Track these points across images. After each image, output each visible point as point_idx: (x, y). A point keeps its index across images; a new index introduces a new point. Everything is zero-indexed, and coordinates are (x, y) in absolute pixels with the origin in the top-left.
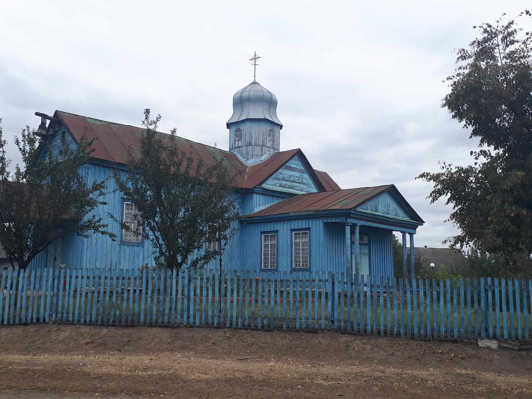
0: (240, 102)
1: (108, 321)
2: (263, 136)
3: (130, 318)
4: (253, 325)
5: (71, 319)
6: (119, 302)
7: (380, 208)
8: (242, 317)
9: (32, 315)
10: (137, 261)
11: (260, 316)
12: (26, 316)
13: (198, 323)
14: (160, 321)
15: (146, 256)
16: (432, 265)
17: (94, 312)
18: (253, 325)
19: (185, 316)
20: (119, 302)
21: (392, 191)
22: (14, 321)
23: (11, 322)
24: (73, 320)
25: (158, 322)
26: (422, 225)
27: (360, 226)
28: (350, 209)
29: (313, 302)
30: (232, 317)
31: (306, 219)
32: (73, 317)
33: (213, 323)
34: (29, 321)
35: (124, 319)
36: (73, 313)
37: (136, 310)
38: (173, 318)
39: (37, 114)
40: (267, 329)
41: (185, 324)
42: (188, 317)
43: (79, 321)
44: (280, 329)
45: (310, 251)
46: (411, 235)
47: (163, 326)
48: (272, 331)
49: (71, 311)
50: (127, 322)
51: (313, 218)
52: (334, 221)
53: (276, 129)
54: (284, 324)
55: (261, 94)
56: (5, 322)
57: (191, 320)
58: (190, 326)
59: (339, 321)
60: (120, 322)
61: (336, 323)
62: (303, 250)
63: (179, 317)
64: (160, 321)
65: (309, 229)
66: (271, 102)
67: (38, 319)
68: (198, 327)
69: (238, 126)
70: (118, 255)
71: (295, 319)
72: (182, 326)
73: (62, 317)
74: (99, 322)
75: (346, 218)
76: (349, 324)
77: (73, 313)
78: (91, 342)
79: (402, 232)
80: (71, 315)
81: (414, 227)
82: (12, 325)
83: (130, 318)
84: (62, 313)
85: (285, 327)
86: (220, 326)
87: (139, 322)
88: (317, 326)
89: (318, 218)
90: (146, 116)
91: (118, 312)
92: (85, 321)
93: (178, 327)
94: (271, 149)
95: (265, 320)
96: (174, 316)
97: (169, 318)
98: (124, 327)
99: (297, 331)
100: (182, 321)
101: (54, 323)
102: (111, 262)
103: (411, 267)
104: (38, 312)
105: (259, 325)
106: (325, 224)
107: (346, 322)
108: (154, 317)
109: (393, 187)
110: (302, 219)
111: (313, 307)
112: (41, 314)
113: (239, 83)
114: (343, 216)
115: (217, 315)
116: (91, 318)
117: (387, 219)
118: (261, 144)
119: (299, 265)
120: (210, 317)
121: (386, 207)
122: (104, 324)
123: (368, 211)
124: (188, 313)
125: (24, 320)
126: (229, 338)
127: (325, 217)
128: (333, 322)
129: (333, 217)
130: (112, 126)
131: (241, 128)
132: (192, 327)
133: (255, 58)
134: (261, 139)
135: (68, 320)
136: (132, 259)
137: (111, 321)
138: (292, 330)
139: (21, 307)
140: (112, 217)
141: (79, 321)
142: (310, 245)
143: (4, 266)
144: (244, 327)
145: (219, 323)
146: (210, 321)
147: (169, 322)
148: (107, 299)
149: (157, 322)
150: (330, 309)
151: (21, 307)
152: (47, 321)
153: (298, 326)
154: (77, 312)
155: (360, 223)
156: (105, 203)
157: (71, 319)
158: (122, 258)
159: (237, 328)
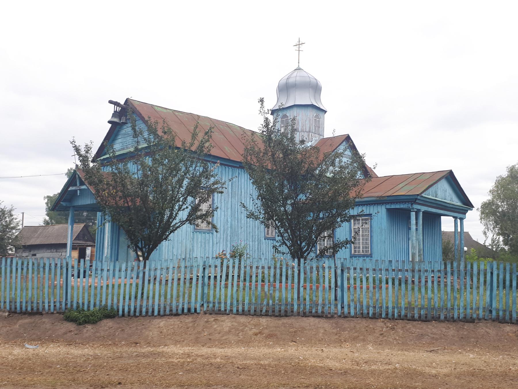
0: (285, 88)
1: (261, 311)
2: (310, 122)
3: (283, 308)
4: (409, 316)
5: (223, 309)
6: (271, 292)
7: (439, 193)
8: (397, 307)
9: (183, 305)
10: (207, 247)
11: (417, 306)
12: (177, 307)
13: (352, 313)
14: (314, 311)
15: (215, 243)
16: (466, 249)
17: (247, 301)
18: (409, 316)
19: (339, 307)
20: (271, 292)
21: (450, 177)
22: (165, 311)
23: (162, 313)
24: (226, 310)
25: (312, 312)
26: (472, 210)
27: (423, 212)
28: (418, 195)
29: (387, 288)
30: (387, 308)
31: (367, 205)
32: (225, 307)
33: (368, 313)
34: (180, 312)
35: (277, 308)
36: (225, 303)
37: (289, 300)
38: (326, 308)
39: (111, 102)
40: (424, 319)
41: (339, 314)
42: (343, 308)
43: (231, 310)
44: (437, 319)
45: (371, 237)
46: (462, 219)
47: (317, 316)
48: (429, 321)
49: (223, 301)
50: (280, 311)
51: (375, 204)
52: (398, 206)
53: (321, 114)
54: (442, 315)
55: (308, 80)
56: (156, 313)
57: (346, 310)
58: (345, 316)
59: (498, 310)
60: (273, 311)
61: (494, 313)
62: (363, 236)
63: (333, 307)
64: (314, 311)
65: (370, 215)
66: (315, 88)
67: (189, 310)
68: (353, 317)
69: (285, 112)
70: (192, 242)
71: (453, 309)
72: (336, 316)
73: (214, 306)
74: (252, 312)
75: (412, 204)
76: (508, 313)
77: (225, 303)
78: (260, 333)
79: (454, 217)
80: (223, 305)
81: (464, 212)
82: (162, 316)
83: (283, 308)
84: (214, 303)
85: (442, 317)
86: (375, 317)
87: (292, 312)
88: (475, 316)
89: (380, 204)
90: (262, 104)
91: (271, 302)
92: (237, 311)
93: (332, 317)
94: (317, 135)
95: (422, 311)
96: (327, 306)
97: (323, 308)
98: (277, 316)
99: (454, 321)
100: (336, 312)
101: (205, 313)
102: (186, 249)
103: (455, 252)
104: (189, 303)
105: (416, 316)
106: (388, 210)
107: (505, 311)
108: (308, 307)
109: (451, 173)
110: (362, 205)
111: (387, 293)
112: (192, 304)
113: (282, 72)
114: (408, 202)
115: (372, 305)
116: (243, 308)
117: (446, 205)
118: (308, 130)
119: (359, 251)
120: (364, 308)
121: (444, 193)
122: (257, 314)
123: (430, 197)
124: (343, 302)
125: (174, 311)
126: (393, 329)
127: (388, 203)
128: (491, 312)
129: (397, 203)
130: (177, 113)
131: (288, 115)
132: (345, 317)
133: (299, 44)
134: (308, 125)
135: (220, 310)
136: (204, 246)
137: (264, 311)
138: (450, 320)
139: (172, 297)
140: (244, 207)
141: (231, 310)
142: (371, 231)
143: (32, 253)
144: (400, 318)
145: (374, 314)
146: (365, 311)
147: (323, 312)
148: (259, 288)
149: (311, 312)
150: (488, 299)
151: (172, 297)
152: (198, 311)
153: (456, 316)
154: (229, 302)
155: (423, 208)
156: (222, 192)
157: (223, 309)
158: (195, 245)
159: (393, 318)
